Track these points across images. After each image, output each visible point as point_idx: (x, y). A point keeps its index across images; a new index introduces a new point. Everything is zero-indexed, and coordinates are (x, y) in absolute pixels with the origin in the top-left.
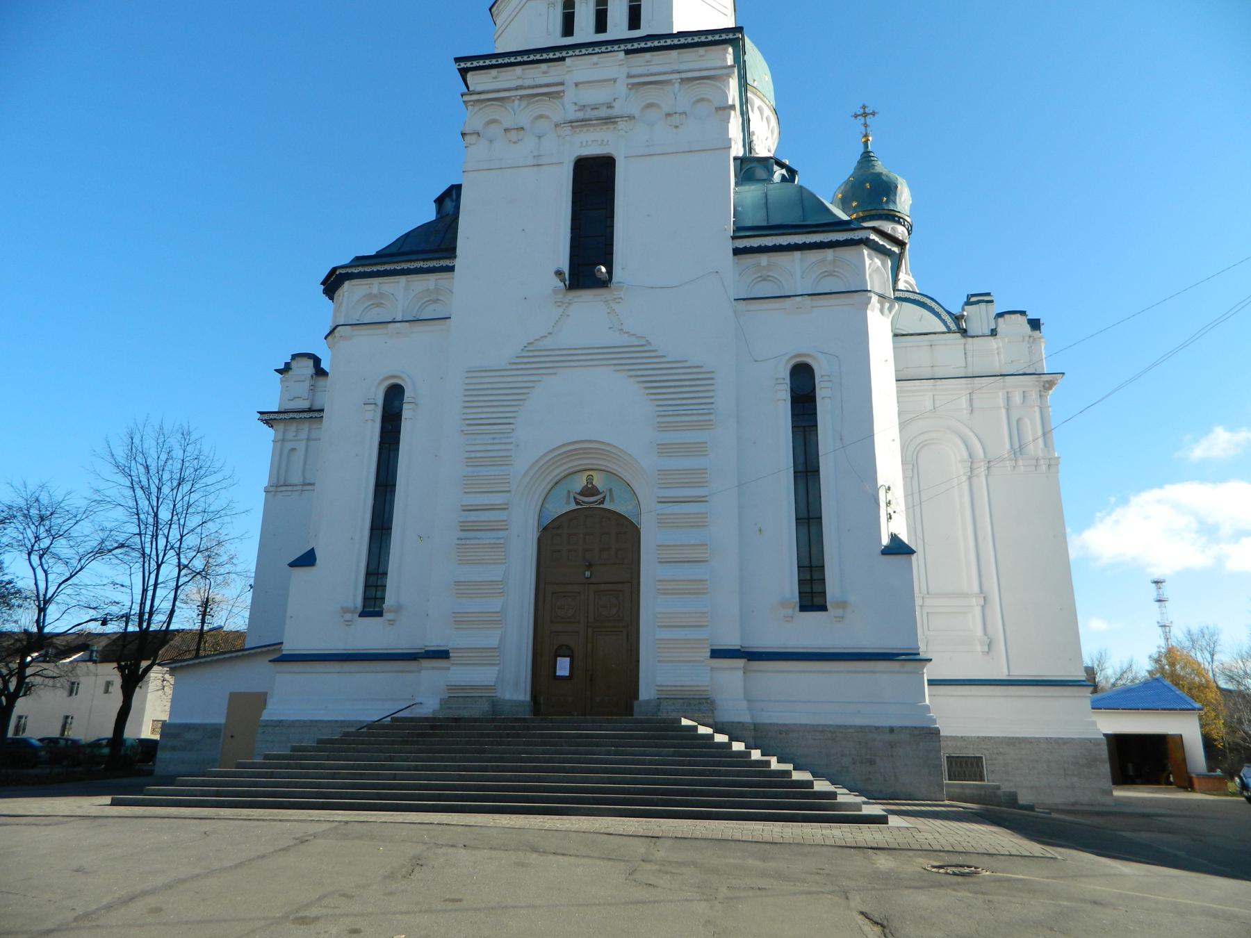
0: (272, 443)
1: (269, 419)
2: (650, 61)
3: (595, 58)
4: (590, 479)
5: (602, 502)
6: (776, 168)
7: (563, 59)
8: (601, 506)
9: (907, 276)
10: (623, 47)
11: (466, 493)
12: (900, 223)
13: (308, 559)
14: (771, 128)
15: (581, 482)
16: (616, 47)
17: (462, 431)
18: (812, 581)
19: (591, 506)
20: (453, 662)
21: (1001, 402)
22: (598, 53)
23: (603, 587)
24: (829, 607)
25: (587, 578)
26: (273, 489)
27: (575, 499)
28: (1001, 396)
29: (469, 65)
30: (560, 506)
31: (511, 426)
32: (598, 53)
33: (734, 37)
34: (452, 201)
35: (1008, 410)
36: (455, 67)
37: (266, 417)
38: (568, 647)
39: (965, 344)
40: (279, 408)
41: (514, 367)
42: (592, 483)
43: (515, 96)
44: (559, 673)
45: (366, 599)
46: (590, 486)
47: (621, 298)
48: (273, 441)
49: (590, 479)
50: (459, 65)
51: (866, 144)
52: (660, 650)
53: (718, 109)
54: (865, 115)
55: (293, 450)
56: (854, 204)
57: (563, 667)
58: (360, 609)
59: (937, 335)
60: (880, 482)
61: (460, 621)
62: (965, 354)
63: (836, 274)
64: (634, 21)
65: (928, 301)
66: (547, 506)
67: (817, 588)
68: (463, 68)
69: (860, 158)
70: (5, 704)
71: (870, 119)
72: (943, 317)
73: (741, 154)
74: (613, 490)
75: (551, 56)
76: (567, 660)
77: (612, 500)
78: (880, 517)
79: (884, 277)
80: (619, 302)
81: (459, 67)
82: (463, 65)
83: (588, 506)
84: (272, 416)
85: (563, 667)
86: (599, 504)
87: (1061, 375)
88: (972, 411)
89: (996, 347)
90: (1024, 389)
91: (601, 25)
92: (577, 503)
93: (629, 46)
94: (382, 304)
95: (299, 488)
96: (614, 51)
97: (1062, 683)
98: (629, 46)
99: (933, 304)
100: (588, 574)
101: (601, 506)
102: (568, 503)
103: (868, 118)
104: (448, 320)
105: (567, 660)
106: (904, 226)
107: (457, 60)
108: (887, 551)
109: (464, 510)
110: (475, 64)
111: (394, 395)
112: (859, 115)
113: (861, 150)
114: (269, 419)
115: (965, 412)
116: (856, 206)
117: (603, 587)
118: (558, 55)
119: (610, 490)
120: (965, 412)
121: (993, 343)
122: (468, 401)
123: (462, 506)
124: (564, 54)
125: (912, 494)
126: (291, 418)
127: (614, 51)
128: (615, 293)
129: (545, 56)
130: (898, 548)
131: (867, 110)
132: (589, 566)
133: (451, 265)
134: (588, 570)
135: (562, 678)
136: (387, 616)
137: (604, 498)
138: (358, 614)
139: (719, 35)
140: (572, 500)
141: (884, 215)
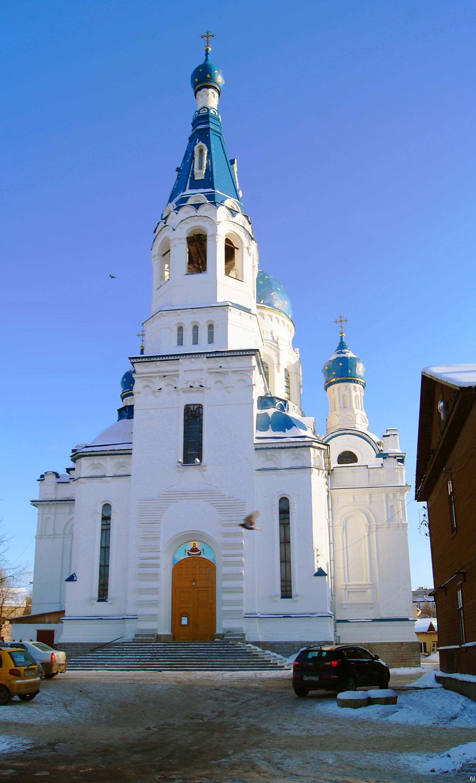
0: (37, 515)
1: (35, 503)
2: (217, 362)
3: (193, 360)
4: (194, 545)
5: (200, 555)
6: (277, 401)
7: (179, 359)
8: (199, 556)
9: (362, 411)
10: (205, 355)
11: (141, 552)
12: (357, 383)
13: (71, 578)
14: (289, 329)
15: (190, 546)
16: (202, 355)
17: (139, 526)
18: (286, 586)
19: (196, 556)
20: (139, 620)
21: (384, 498)
22: (194, 358)
23: (199, 589)
24: (292, 597)
25: (194, 586)
26: (40, 537)
27: (188, 553)
28: (384, 495)
29: (135, 361)
30: (181, 556)
31: (159, 524)
32: (194, 358)
33: (255, 353)
34: (126, 412)
35: (387, 501)
36: (129, 361)
37: (34, 503)
38: (186, 613)
39: (368, 472)
40: (40, 498)
41: (159, 499)
42: (195, 547)
43: (157, 376)
44: (183, 623)
45: (99, 595)
46: (194, 548)
47: (206, 470)
48: (38, 514)
49: (194, 545)
50: (131, 361)
51: (341, 337)
52: (224, 615)
53: (248, 386)
54: (341, 321)
55: (48, 518)
56: (334, 373)
57: (184, 621)
58: (97, 599)
59: (356, 467)
60: (315, 547)
61: (142, 604)
62: (369, 476)
63: (404, 661)
64: (211, 340)
65: (364, 436)
66: (176, 556)
67: (288, 589)
68: (133, 362)
69: (338, 345)
70: (325, 664)
71: (343, 324)
72: (371, 443)
73: (263, 394)
74: (204, 549)
75: (173, 358)
76: (186, 618)
77: (204, 553)
78: (416, 475)
79: (320, 459)
80: (205, 471)
81: (131, 362)
82: (132, 361)
83: (194, 556)
84: (37, 503)
85: (184, 621)
86: (198, 555)
87: (410, 487)
88: (371, 502)
89: (382, 472)
90: (394, 493)
91: (195, 342)
92: (189, 555)
93: (208, 355)
94: (99, 467)
95: (52, 537)
96: (201, 357)
97: (404, 620)
98: (208, 355)
99: (367, 437)
100: (194, 584)
101: (199, 556)
102: (185, 555)
103: (342, 323)
104: (130, 477)
105: (186, 618)
106: (360, 384)
107: (130, 358)
108: (316, 575)
109: (141, 559)
110: (138, 360)
111: (284, 501)
112: (338, 321)
113: (339, 341)
114: (35, 503)
115: (368, 503)
116: (334, 375)
117: (199, 589)
118: (176, 358)
119: (203, 549)
120: (368, 503)
121: (382, 471)
122: (141, 516)
123: (140, 558)
124: (179, 357)
125: (327, 554)
126: (47, 504)
127: (201, 357)
128: (204, 468)
129: (170, 358)
130: (321, 573)
131: (342, 319)
132: (194, 580)
133: (130, 452)
134: (194, 582)
135: (185, 625)
136: (110, 601)
137: (201, 553)
138: (97, 601)
139: (248, 352)
140: (187, 553)
141: (349, 380)
